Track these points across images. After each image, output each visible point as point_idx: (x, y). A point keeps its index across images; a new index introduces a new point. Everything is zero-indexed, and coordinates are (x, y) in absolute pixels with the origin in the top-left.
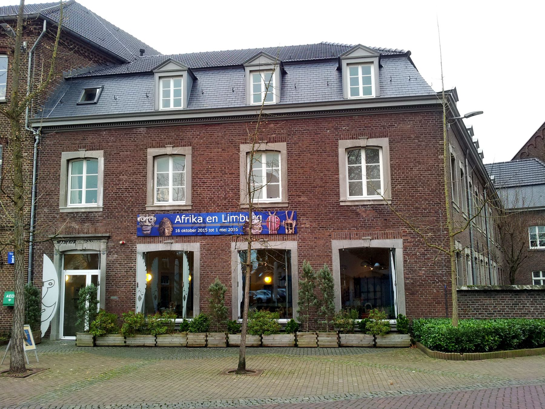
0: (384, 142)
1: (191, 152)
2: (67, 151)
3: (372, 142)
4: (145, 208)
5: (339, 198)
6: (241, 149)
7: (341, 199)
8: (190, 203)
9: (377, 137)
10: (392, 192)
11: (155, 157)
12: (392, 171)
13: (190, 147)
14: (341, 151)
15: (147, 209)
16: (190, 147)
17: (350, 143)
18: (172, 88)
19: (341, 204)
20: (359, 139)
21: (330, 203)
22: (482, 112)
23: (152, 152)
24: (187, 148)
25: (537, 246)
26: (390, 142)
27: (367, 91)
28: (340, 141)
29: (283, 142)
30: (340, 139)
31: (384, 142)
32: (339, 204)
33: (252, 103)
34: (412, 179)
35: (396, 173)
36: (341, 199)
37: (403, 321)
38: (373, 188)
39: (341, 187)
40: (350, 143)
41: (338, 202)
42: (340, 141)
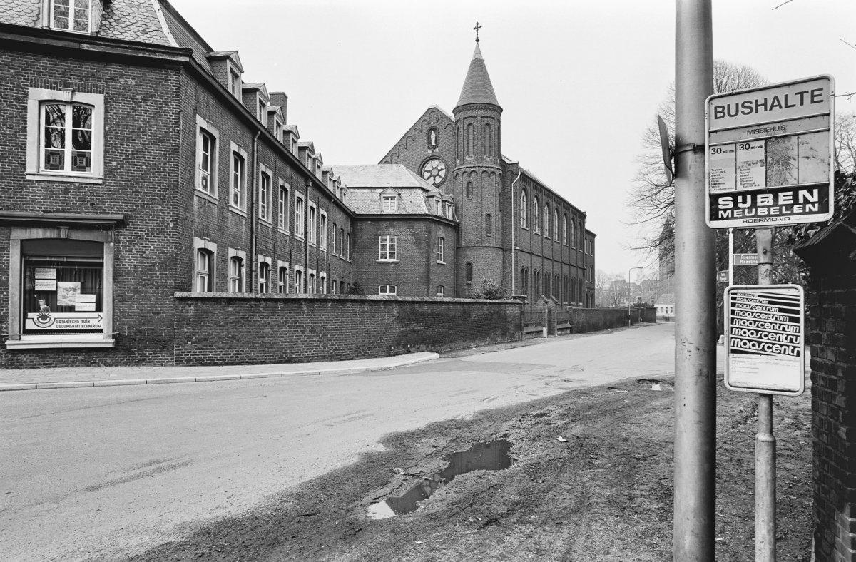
0: (97, 100)
3: (81, 97)
7: (28, 172)
9: (88, 92)
10: (105, 168)
12: (106, 140)
14: (32, 105)
15: (791, 193)
17: (46, 94)
19: (28, 177)
20: (60, 90)
21: (10, 174)
22: (795, 105)
25: (386, 258)
26: (106, 101)
30: (31, 86)
31: (97, 100)
32: (24, 178)
35: (112, 144)
36: (28, 172)
37: (835, 373)
38: (81, 162)
40: (46, 94)
41: (23, 175)
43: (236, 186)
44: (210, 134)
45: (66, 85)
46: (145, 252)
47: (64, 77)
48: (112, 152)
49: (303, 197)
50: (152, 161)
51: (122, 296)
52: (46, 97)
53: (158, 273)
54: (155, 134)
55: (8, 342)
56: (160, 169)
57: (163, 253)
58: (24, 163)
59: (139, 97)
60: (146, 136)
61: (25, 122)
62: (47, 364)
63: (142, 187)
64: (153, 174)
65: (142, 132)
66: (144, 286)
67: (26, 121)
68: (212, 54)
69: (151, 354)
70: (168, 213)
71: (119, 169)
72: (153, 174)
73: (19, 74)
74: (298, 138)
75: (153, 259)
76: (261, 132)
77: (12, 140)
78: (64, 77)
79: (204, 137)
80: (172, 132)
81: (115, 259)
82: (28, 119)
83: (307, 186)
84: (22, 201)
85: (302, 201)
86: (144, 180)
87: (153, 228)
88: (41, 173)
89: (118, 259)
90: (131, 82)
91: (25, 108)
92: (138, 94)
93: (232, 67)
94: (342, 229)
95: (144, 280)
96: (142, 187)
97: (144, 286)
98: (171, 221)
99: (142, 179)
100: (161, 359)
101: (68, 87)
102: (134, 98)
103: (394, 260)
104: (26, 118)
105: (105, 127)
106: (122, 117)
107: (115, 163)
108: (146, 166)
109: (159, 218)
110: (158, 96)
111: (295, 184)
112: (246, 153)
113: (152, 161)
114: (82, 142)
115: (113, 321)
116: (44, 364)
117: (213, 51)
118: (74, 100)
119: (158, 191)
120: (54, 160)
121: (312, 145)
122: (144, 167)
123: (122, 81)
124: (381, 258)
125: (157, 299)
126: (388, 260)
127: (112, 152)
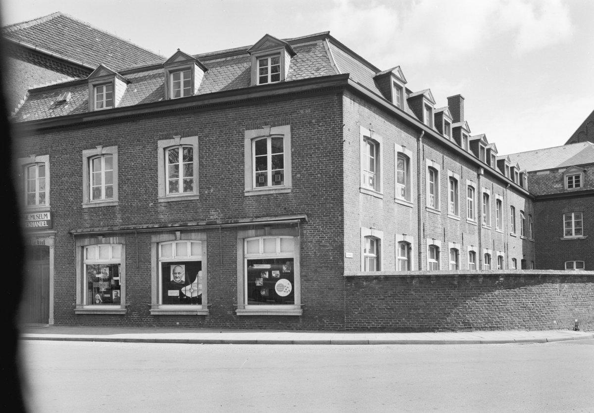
0: (285, 131)
1: (117, 150)
2: (163, 139)
4: (157, 200)
5: (244, 189)
6: (159, 146)
8: (198, 194)
11: (89, 158)
13: (117, 147)
14: (247, 142)
16: (117, 147)
18: (182, 80)
19: (246, 194)
20: (263, 128)
23: (86, 153)
24: (113, 147)
25: (571, 235)
26: (292, 130)
27: (178, 93)
28: (246, 131)
29: (45, 154)
30: (246, 130)
31: (285, 131)
33: (96, 109)
34: (311, 166)
36: (246, 189)
38: (278, 178)
39: (291, 172)
42: (246, 131)
43: (485, 213)
44: (374, 141)
45: (266, 124)
46: (321, 242)
47: (265, 118)
48: (297, 167)
49: (475, 185)
50: (325, 169)
51: (307, 276)
52: (254, 136)
53: (331, 258)
54: (325, 148)
55: (152, 310)
56: (330, 175)
57: (334, 241)
58: (243, 184)
59: (314, 121)
60: (319, 150)
61: (243, 155)
62: (260, 327)
63: (319, 191)
64: (326, 180)
65: (317, 148)
66: (321, 267)
67: (244, 155)
68: (411, 95)
69: (328, 321)
70: (337, 209)
71: (302, 179)
72: (326, 180)
73: (240, 123)
74: (434, 103)
75: (327, 247)
76: (425, 131)
77: (237, 170)
78: (265, 118)
79: (430, 171)
80: (338, 144)
81: (301, 248)
82: (245, 154)
83: (479, 175)
84: (318, 223)
85: (474, 189)
86: (319, 185)
87: (326, 223)
88: (254, 190)
89: (303, 248)
90: (308, 111)
91: (243, 146)
92: (313, 119)
93: (427, 103)
94: (529, 215)
95: (323, 263)
96: (319, 191)
97: (321, 267)
98: (340, 215)
99: (318, 185)
100: (335, 326)
101: (268, 125)
102: (310, 123)
103: (581, 236)
104: (244, 153)
105: (292, 148)
106: (302, 139)
107: (299, 175)
108: (320, 174)
109: (330, 214)
110: (328, 116)
111: (465, 175)
112: (411, 152)
113: (325, 169)
114: (278, 162)
115: (301, 295)
116: (258, 327)
117: (380, 71)
118: (271, 133)
119: (330, 192)
120: (261, 181)
121: (485, 137)
122: (319, 175)
123: (302, 112)
124: (566, 235)
125: (331, 278)
126: (574, 236)
127: (297, 167)
